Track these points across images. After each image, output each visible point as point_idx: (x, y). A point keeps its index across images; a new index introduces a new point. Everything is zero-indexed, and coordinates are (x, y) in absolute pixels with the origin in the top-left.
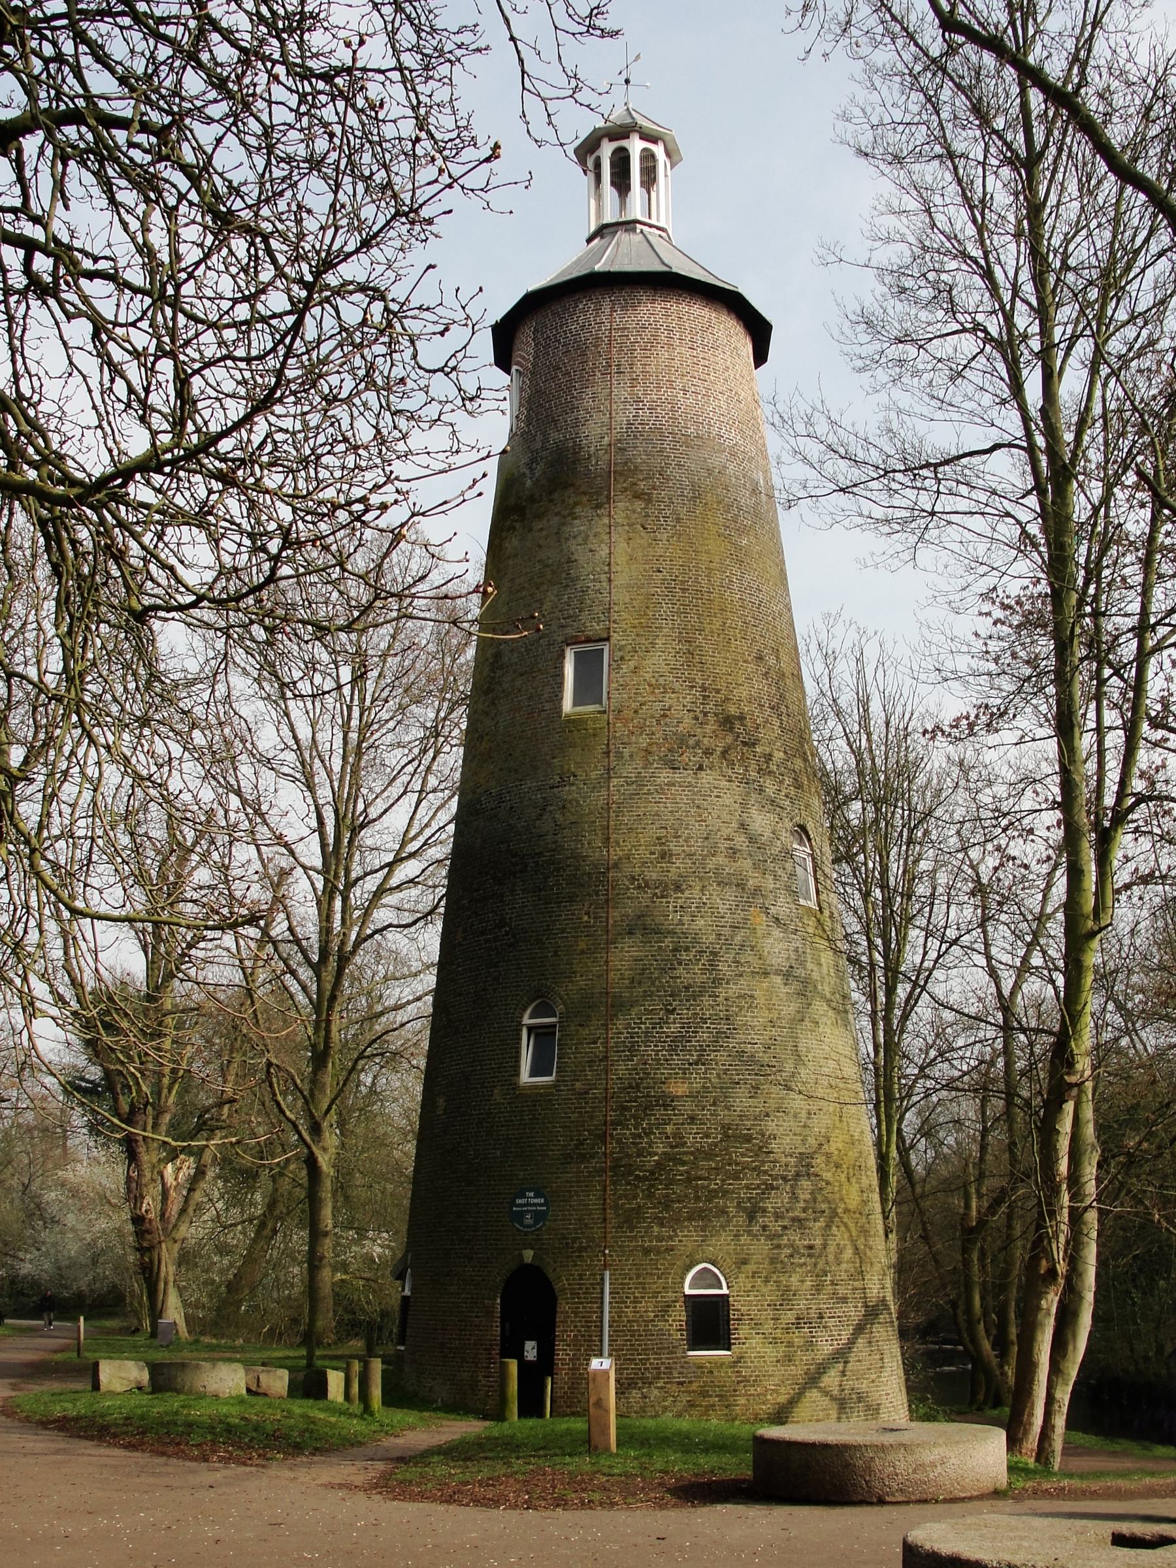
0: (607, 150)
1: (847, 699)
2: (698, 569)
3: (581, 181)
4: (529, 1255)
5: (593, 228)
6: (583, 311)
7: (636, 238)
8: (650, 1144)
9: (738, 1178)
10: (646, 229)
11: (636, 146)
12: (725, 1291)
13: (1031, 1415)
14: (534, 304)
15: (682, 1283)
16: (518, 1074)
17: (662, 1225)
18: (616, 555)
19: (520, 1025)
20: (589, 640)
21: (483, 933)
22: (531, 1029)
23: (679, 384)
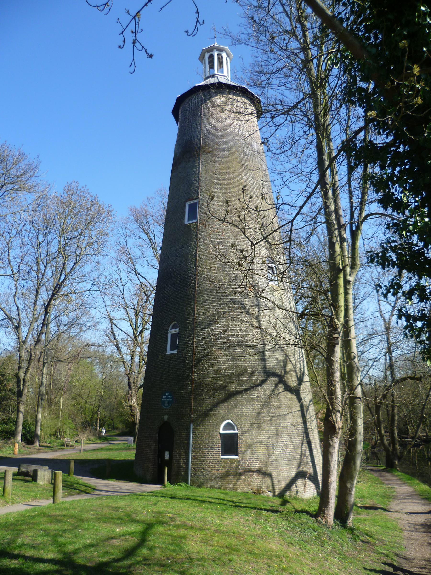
0: (207, 55)
2: (229, 172)
3: (201, 66)
6: (194, 100)
12: (236, 431)
14: (180, 101)
15: (219, 428)
18: (207, 172)
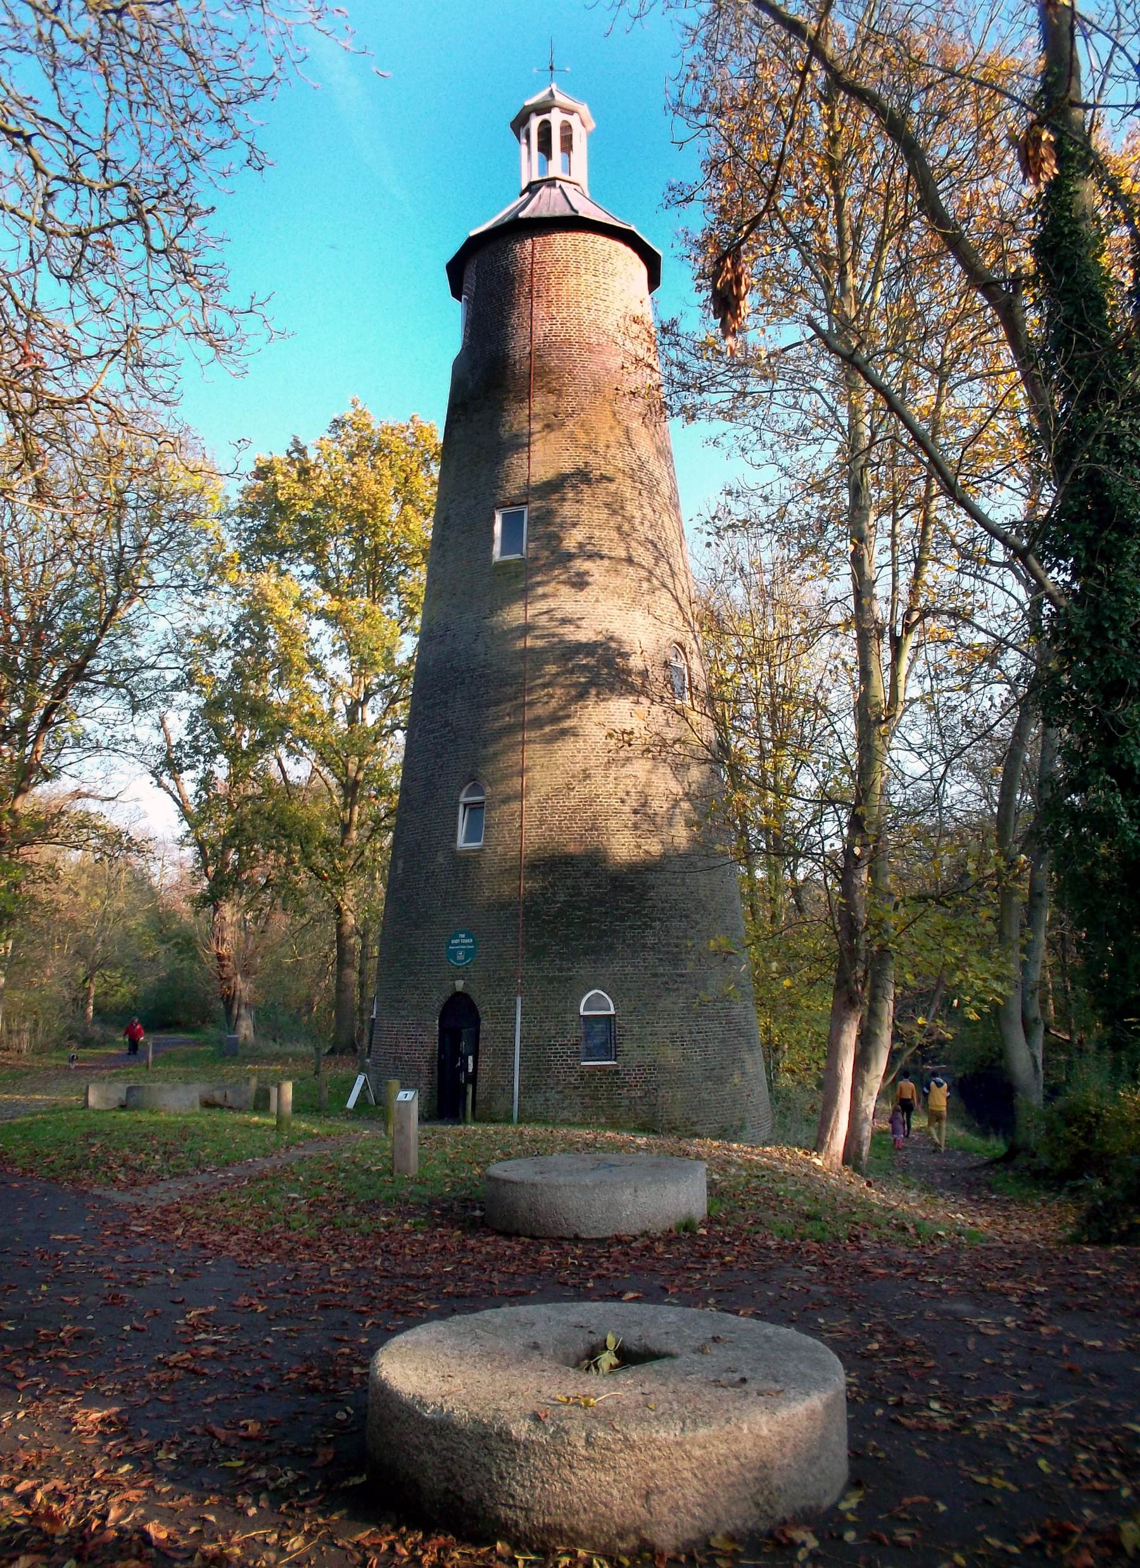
0: (535, 122)
1: (529, 714)
4: (460, 984)
5: (524, 185)
7: (556, 192)
8: (554, 894)
9: (623, 921)
10: (564, 184)
11: (556, 118)
13: (836, 1121)
14: (474, 246)
16: (455, 841)
17: (562, 959)
19: (457, 803)
20: (513, 504)
21: (433, 732)
22: (465, 805)
23: (584, 304)
